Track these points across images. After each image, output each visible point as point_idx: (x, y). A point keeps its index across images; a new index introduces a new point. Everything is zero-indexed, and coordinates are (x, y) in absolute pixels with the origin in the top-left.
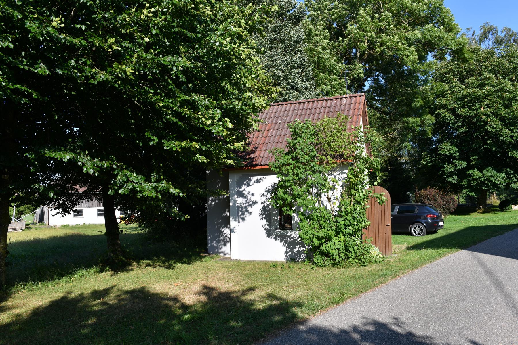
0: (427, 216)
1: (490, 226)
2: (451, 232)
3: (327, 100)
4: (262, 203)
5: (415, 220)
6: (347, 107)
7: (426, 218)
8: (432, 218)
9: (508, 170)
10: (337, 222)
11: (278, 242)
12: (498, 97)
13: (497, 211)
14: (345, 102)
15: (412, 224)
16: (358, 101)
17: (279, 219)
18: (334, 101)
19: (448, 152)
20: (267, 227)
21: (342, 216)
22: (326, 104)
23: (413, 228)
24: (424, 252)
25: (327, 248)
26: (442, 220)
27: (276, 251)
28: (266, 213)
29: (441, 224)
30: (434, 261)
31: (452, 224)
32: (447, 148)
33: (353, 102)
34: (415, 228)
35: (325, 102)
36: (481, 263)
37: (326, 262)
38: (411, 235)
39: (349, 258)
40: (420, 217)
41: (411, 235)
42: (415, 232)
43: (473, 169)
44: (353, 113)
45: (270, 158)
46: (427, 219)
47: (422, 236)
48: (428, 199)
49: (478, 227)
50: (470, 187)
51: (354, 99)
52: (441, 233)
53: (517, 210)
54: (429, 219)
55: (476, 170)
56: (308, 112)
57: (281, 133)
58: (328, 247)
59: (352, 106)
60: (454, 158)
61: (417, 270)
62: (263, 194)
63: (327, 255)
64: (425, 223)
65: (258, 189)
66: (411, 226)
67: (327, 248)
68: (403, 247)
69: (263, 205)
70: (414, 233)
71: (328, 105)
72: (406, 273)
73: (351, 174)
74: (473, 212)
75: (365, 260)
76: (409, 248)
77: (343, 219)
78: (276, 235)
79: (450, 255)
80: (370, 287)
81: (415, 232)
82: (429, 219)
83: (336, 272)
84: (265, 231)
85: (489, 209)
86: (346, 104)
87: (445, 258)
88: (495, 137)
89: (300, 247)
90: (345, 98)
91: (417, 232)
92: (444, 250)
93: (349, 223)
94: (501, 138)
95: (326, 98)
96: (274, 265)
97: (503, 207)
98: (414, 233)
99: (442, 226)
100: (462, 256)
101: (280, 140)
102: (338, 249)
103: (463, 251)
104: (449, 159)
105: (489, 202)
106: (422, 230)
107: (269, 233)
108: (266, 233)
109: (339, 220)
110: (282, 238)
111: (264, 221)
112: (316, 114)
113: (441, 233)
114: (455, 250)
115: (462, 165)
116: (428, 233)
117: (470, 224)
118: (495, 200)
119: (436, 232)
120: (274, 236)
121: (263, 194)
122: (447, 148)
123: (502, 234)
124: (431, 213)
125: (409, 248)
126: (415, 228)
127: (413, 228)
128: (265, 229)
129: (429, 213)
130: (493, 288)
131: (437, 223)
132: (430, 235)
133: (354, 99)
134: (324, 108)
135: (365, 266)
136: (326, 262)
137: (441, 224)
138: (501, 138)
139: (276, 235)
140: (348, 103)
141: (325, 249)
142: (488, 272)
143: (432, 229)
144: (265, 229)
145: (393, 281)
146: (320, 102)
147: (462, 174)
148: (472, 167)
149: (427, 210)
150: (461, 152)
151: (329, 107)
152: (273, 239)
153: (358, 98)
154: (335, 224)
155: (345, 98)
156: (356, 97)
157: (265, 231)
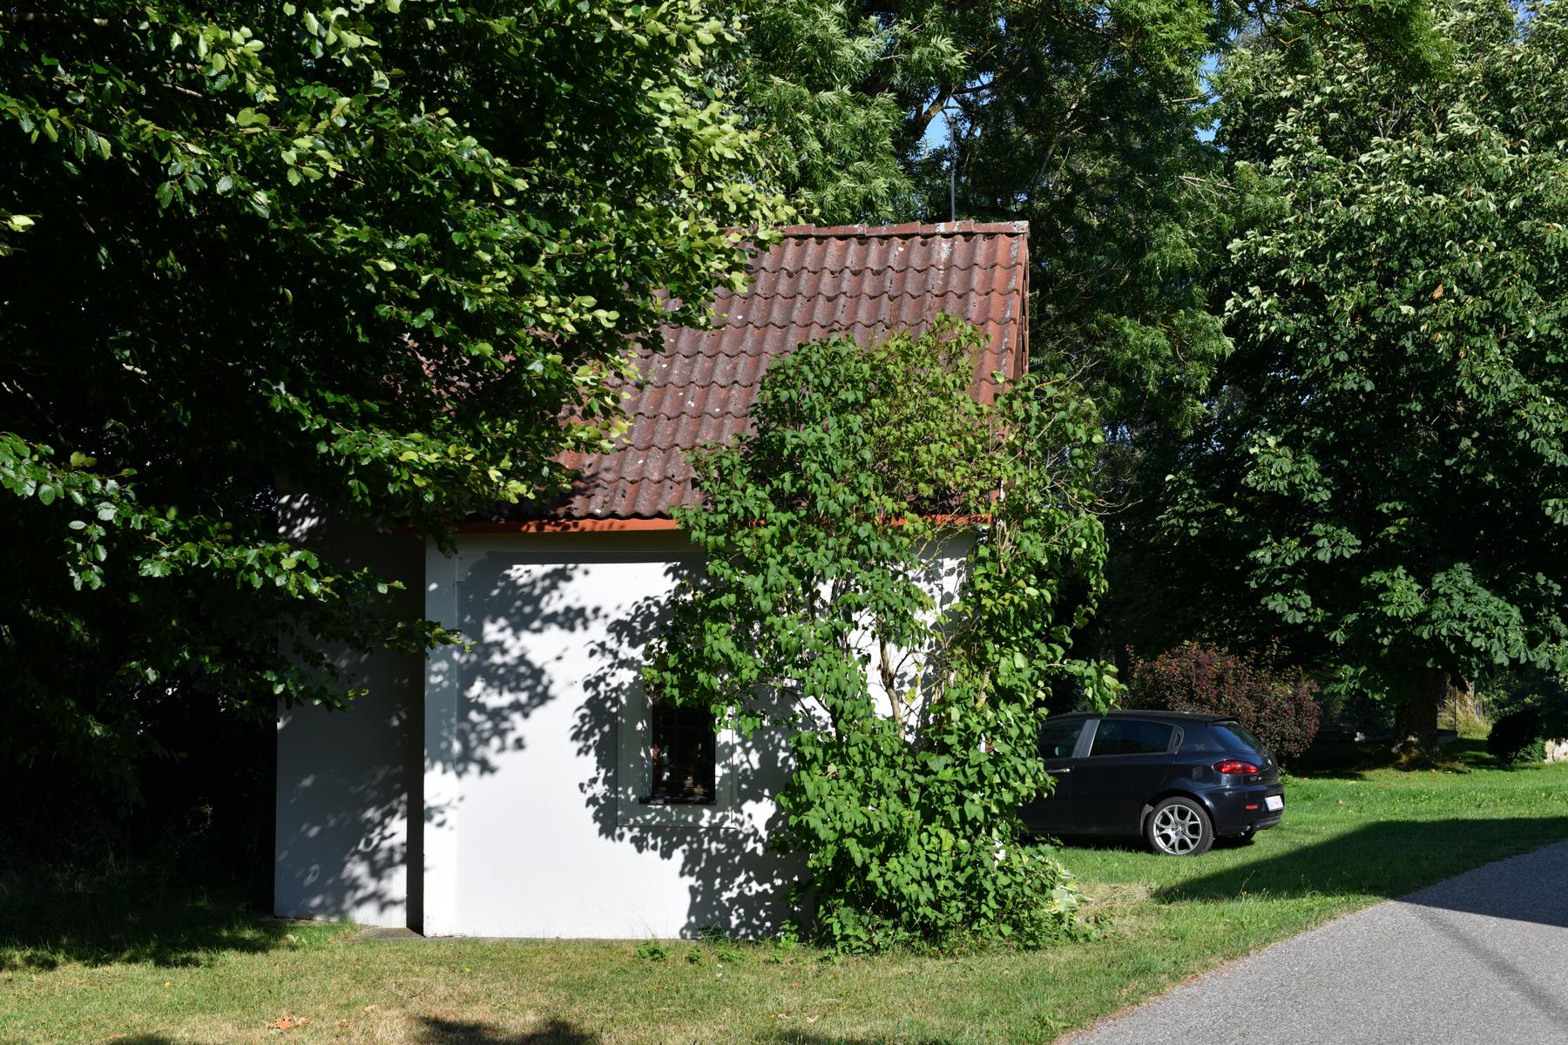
0: (1219, 767)
1: (1465, 822)
2: (1309, 840)
3: (863, 239)
4: (587, 685)
5: (1166, 785)
6: (955, 280)
7: (1210, 776)
8: (1242, 778)
9: (1541, 578)
10: (925, 770)
11: (652, 856)
12: (1521, 240)
13: (1480, 763)
14: (944, 255)
15: (1155, 802)
16: (1000, 258)
17: (659, 757)
18: (898, 248)
19: (1283, 484)
20: (600, 789)
21: (945, 749)
22: (863, 258)
23: (1158, 820)
24: (1250, 907)
25: (889, 876)
26: (1277, 790)
27: (649, 895)
28: (601, 723)
29: (1274, 803)
30: (1295, 933)
31: (1312, 811)
32: (1274, 461)
33: (980, 258)
34: (1166, 821)
35: (854, 245)
36: (1468, 943)
37: (878, 937)
38: (1151, 849)
39: (977, 916)
40: (1186, 771)
41: (1151, 849)
42: (1166, 838)
43: (1388, 566)
44: (986, 308)
45: (630, 489)
46: (1218, 780)
47: (1196, 853)
48: (1191, 697)
49: (1414, 824)
50: (1360, 648)
51: (983, 246)
52: (1266, 845)
53: (1564, 764)
54: (1225, 781)
55: (1401, 570)
56: (783, 286)
57: (667, 373)
58: (901, 874)
59: (977, 277)
60: (1313, 512)
61: (1248, 960)
62: (602, 645)
63: (889, 907)
64: (1210, 796)
65: (590, 620)
66: (1148, 808)
67: (889, 876)
68: (1139, 892)
69: (590, 693)
70: (1160, 842)
71: (873, 262)
72: (1214, 966)
73: (987, 576)
74: (1372, 767)
75: (1038, 927)
76: (1168, 895)
77: (946, 759)
78: (645, 828)
79: (1349, 917)
80: (1115, 1005)
81: (1166, 838)
82: (1225, 781)
83: (934, 968)
84: (592, 809)
85: (1447, 751)
86: (949, 266)
87: (1331, 924)
88: (1500, 433)
89: (748, 880)
90: (945, 236)
91: (1174, 838)
92: (1319, 899)
93: (973, 779)
94: (1521, 435)
95: (859, 228)
96: (655, 951)
97: (1509, 745)
98: (1160, 842)
99: (1278, 812)
100: (1383, 920)
101: (667, 408)
102: (931, 881)
103: (1391, 903)
104: (1284, 513)
105: (1444, 720)
106: (1194, 829)
107: (609, 819)
108: (596, 818)
109: (936, 762)
110: (668, 838)
111: (591, 759)
112: (821, 300)
113: (1266, 845)
114: (1368, 898)
115: (1337, 543)
116: (1221, 843)
117: (1383, 813)
118: (1469, 715)
119: (1246, 841)
120: (636, 831)
121: (602, 645)
122: (1274, 461)
123: (1520, 851)
124: (1235, 755)
125: (1168, 895)
126: (1166, 821)
127: (1158, 820)
128: (592, 801)
129: (1227, 753)
130: (1531, 1009)
131: (1260, 798)
132: (1227, 853)
133: (983, 246)
134: (855, 273)
135: (1036, 948)
136: (878, 937)
137: (1274, 803)
138: (1521, 435)
139: (645, 828)
140: (959, 260)
141: (879, 881)
142: (1503, 968)
143: (1234, 823)
144: (592, 801)
145: (1177, 990)
146: (834, 246)
147: (1337, 585)
148: (1386, 558)
149: (1221, 740)
150: (1343, 484)
151: (877, 273)
152: (626, 846)
153: (1002, 241)
154: (920, 779)
155: (945, 236)
156: (990, 236)
157: (592, 809)
